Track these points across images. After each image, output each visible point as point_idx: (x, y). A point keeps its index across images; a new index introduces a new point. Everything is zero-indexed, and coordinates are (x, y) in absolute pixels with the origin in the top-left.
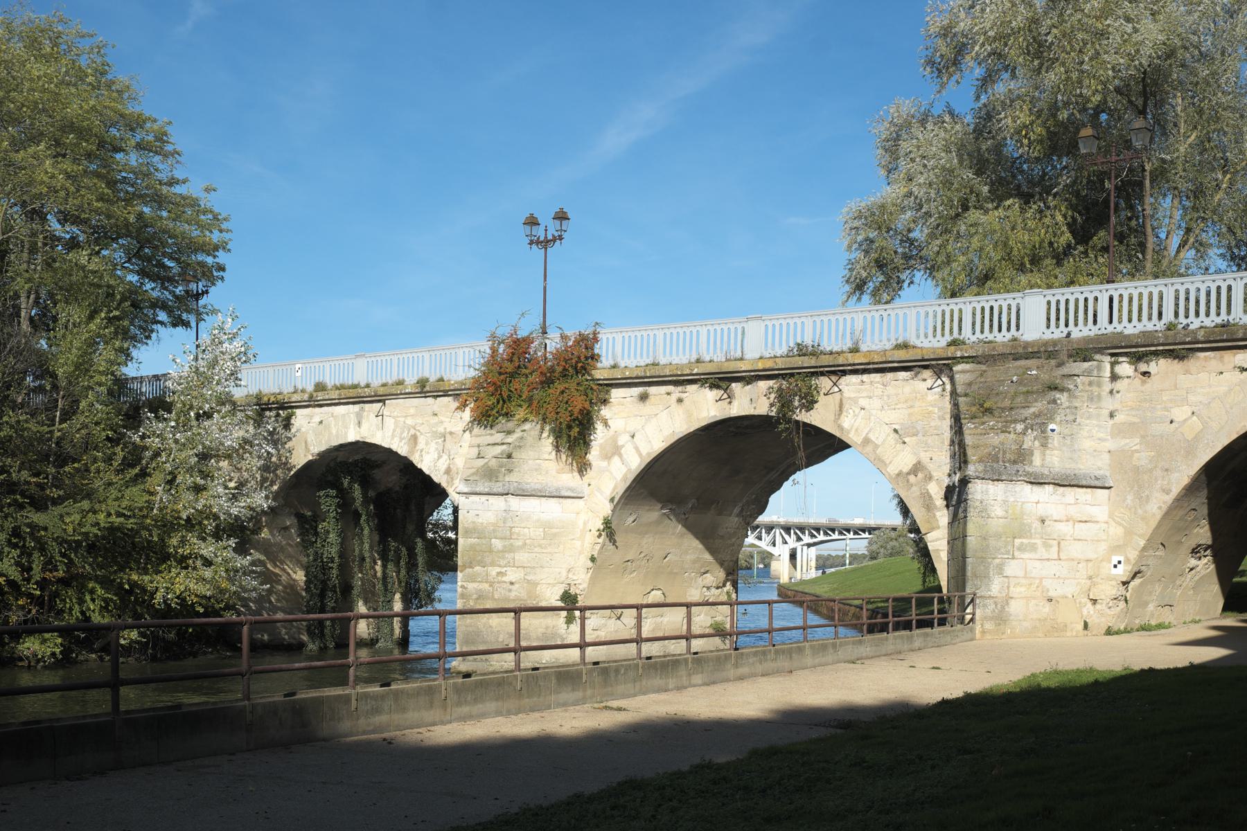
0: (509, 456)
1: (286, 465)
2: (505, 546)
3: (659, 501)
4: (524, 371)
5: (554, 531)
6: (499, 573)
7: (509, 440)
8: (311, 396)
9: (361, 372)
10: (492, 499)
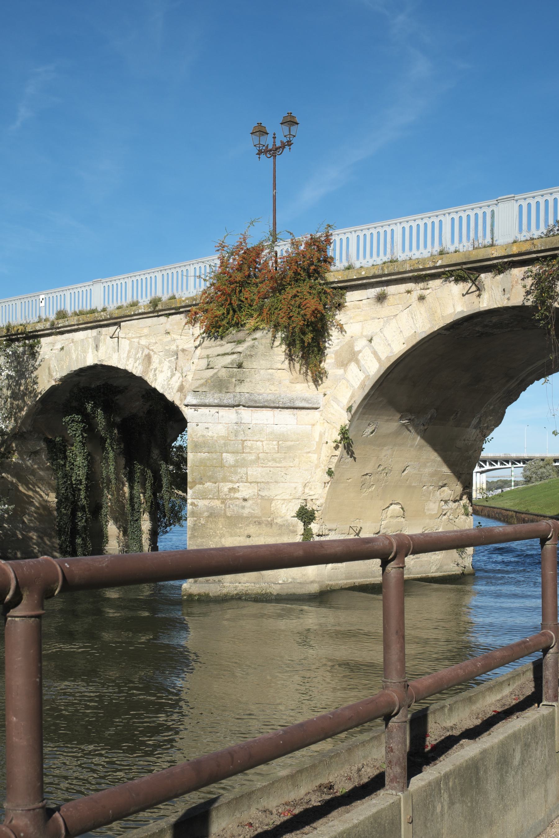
0: (240, 366)
1: (34, 393)
2: (237, 461)
3: (399, 411)
4: (254, 280)
5: (289, 443)
6: (231, 490)
7: (240, 349)
8: (53, 324)
9: (98, 296)
10: (223, 412)
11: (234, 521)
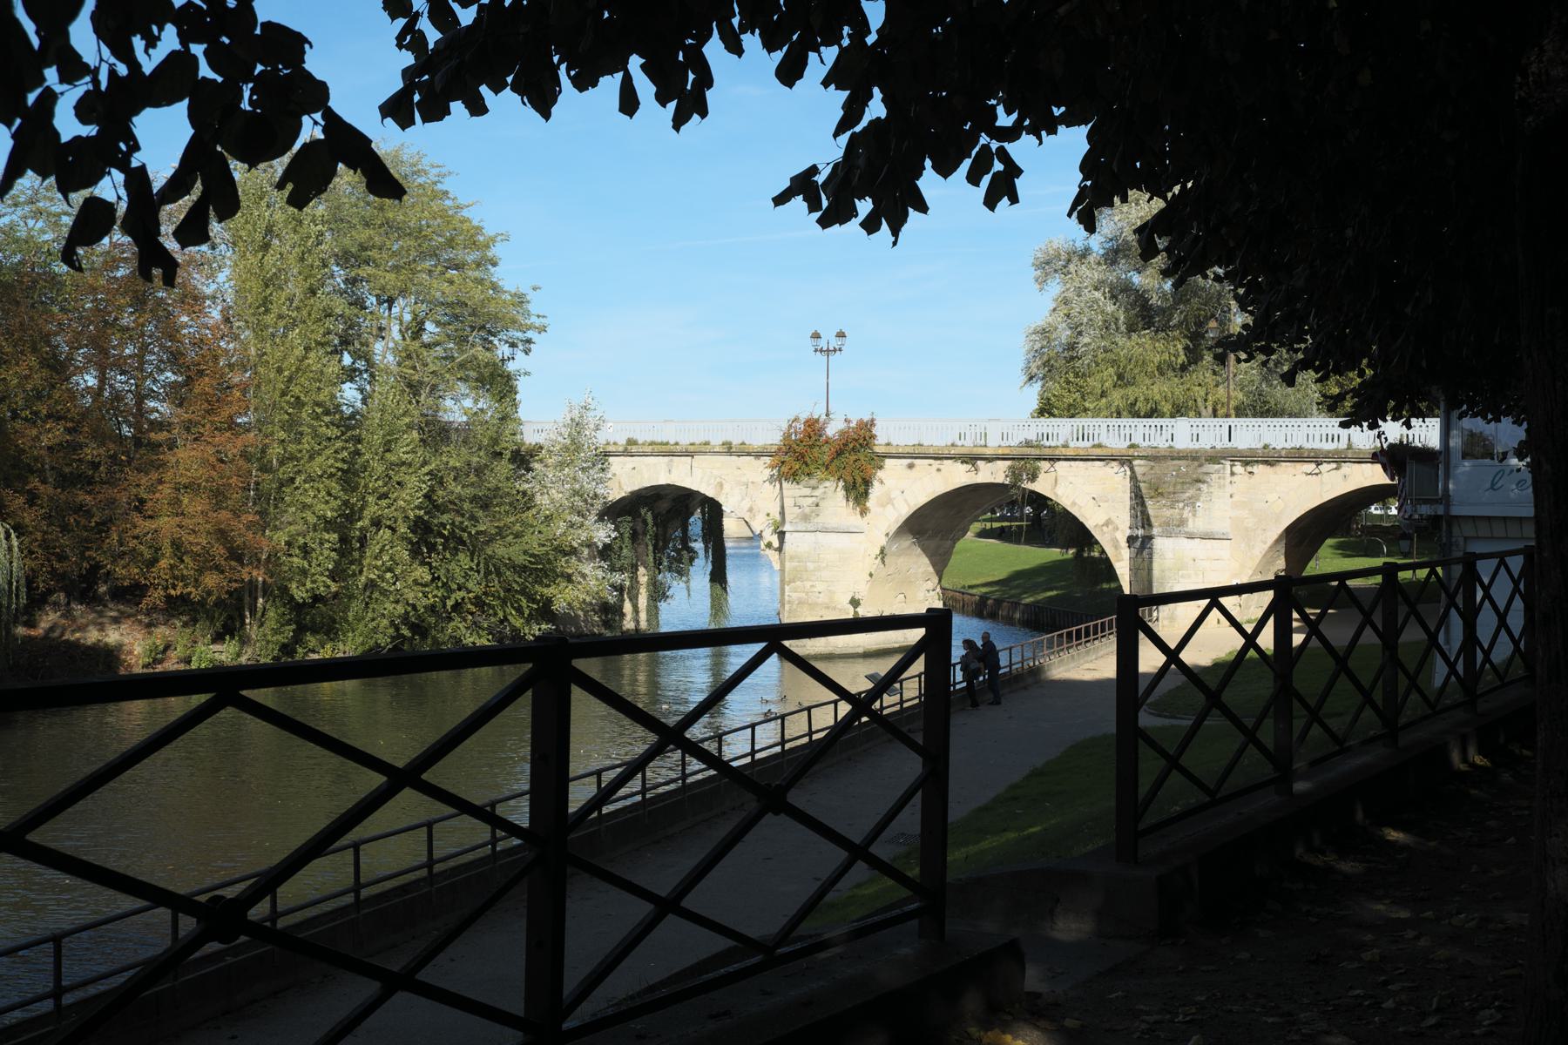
11: (813, 606)
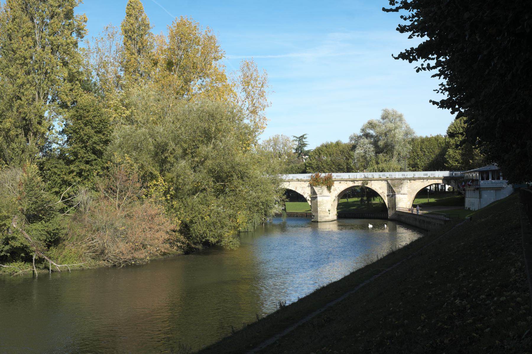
11: (416, 190)
